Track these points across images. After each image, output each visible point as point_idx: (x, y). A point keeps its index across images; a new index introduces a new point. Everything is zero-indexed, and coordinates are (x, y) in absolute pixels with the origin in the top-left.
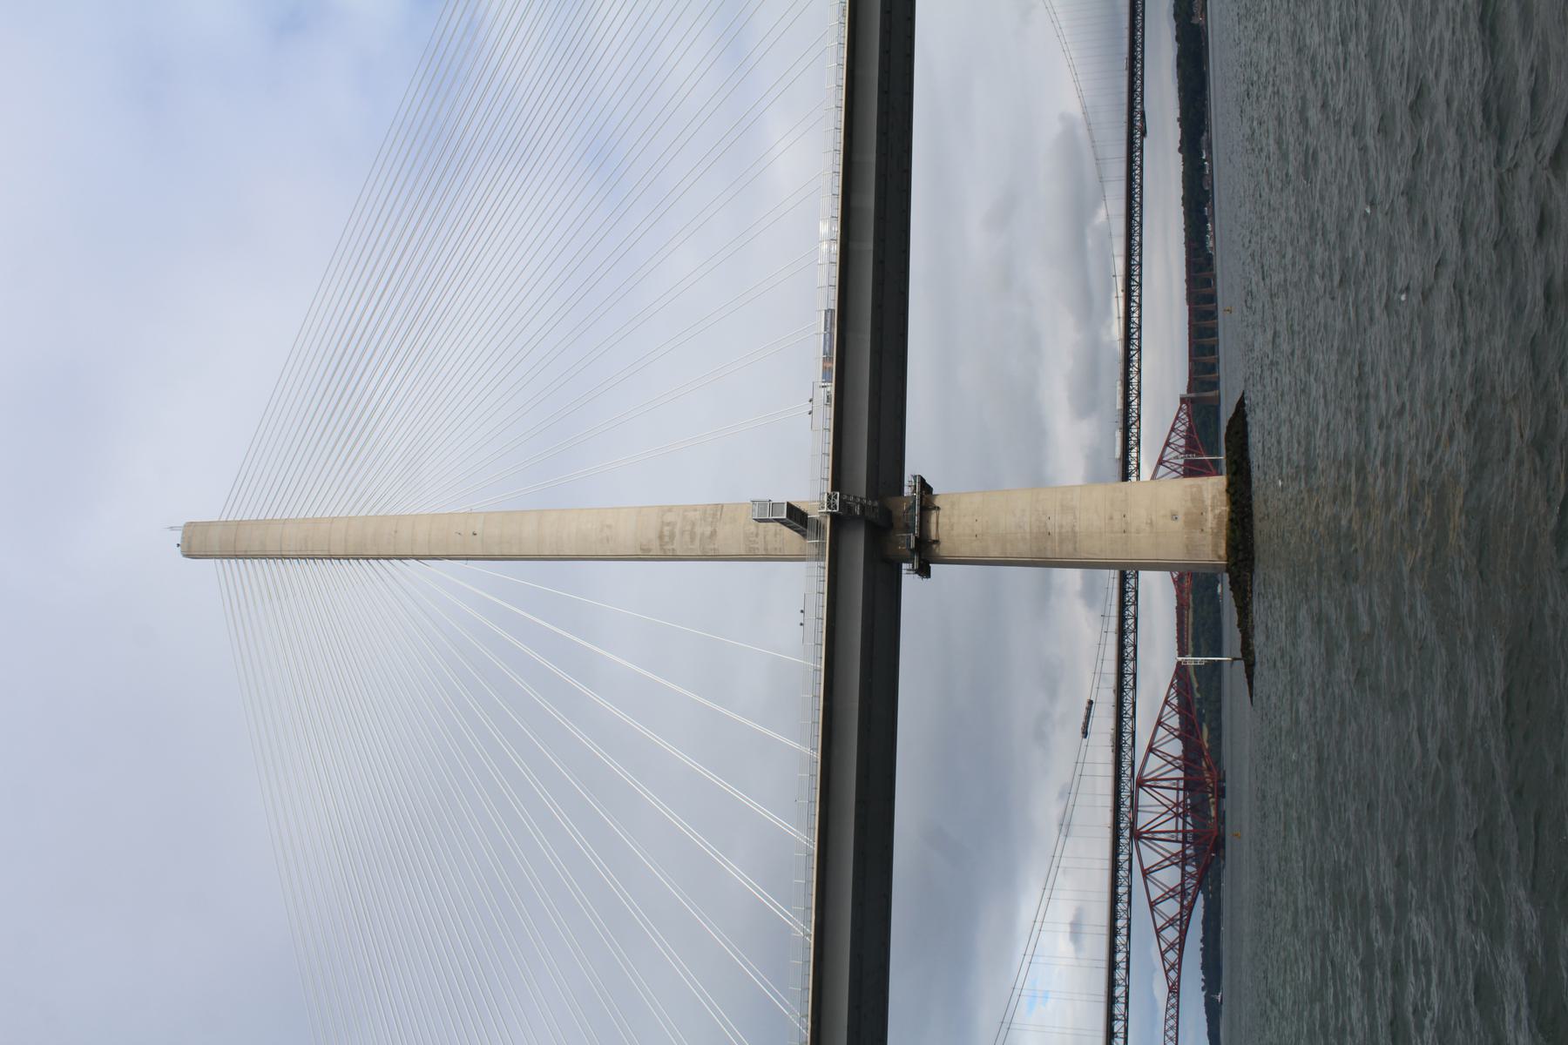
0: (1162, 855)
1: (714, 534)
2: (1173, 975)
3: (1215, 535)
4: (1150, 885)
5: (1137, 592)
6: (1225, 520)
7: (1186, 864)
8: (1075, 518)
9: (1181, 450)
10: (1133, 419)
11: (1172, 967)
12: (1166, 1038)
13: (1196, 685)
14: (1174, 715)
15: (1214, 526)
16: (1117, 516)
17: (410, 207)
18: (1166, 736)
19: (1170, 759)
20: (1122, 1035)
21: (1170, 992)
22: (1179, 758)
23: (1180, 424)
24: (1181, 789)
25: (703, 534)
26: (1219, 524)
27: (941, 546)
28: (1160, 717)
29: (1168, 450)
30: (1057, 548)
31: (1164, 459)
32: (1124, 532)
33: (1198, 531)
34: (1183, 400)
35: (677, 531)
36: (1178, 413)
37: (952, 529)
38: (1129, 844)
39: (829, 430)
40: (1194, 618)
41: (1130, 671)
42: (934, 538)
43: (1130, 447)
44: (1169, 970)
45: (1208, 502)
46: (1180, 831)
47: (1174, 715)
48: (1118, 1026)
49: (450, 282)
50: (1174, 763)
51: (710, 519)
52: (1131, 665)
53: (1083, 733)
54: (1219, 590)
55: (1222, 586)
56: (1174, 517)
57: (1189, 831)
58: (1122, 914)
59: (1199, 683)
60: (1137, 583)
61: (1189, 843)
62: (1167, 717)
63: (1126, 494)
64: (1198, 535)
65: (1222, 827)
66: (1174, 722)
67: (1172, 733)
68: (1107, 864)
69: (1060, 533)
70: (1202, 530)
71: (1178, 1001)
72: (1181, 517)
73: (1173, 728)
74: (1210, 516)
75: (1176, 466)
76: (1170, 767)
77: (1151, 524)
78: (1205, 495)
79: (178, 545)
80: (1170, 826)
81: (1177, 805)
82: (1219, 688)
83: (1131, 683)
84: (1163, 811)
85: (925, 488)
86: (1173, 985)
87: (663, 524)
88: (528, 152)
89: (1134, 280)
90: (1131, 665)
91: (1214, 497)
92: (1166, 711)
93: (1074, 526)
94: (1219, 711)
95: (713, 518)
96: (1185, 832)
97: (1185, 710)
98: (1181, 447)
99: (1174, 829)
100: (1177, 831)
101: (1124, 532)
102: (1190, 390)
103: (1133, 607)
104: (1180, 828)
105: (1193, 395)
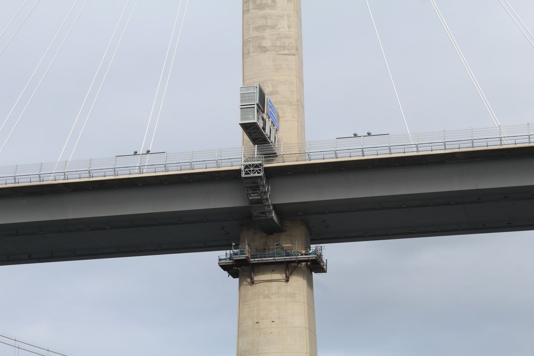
1: (264, 49)
25: (263, 38)
35: (267, 11)
42: (256, 278)
95: (280, 46)
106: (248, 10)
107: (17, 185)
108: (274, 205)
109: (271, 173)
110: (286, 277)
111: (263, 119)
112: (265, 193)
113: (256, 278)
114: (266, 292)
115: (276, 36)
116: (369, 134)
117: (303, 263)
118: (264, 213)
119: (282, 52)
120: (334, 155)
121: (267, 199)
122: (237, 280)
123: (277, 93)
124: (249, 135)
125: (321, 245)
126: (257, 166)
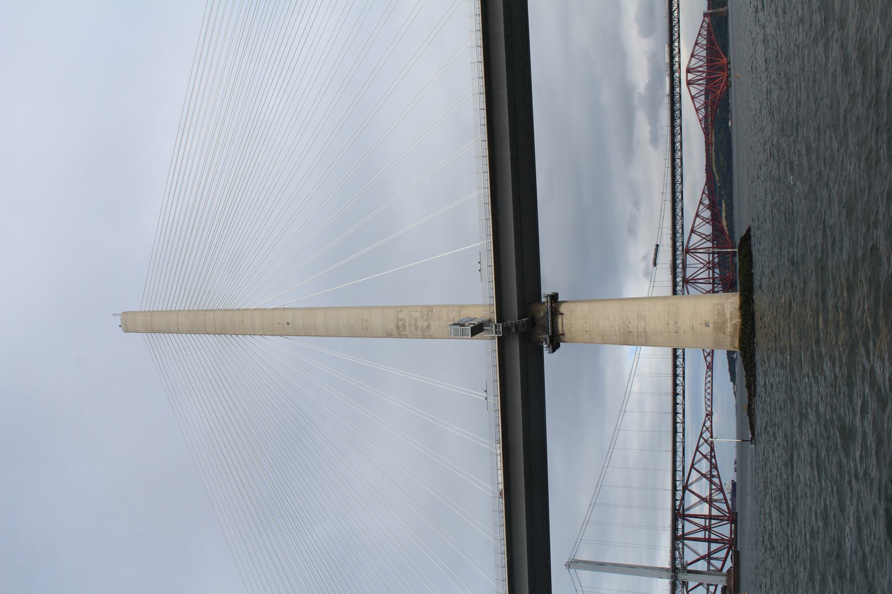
0: (700, 103)
1: (429, 326)
2: (709, 359)
3: (732, 336)
4: (695, 102)
5: (680, 96)
6: (738, 327)
7: (715, 268)
8: (646, 323)
9: (705, 29)
10: (675, 7)
11: (709, 354)
12: (706, 393)
13: (717, 179)
14: (705, 210)
15: (732, 331)
16: (672, 322)
17: (191, 262)
18: (702, 223)
19: (704, 236)
20: (682, 357)
21: (708, 368)
22: (709, 236)
23: (704, 30)
24: (711, 253)
25: (422, 326)
26: (735, 330)
27: (566, 336)
28: (697, 212)
29: (697, 47)
30: (636, 340)
31: (695, 54)
32: (676, 332)
33: (722, 333)
34: (705, 15)
35: (407, 324)
36: (702, 24)
37: (572, 327)
38: (681, 236)
39: (482, 78)
40: (715, 139)
41: (679, 157)
42: (561, 332)
43: (674, 24)
44: (707, 356)
45: (728, 316)
46: (711, 278)
47: (705, 210)
48: (679, 371)
49: (228, 198)
50: (706, 238)
51: (426, 318)
52: (679, 153)
53: (654, 264)
54: (730, 125)
55: (731, 122)
56: (707, 325)
57: (716, 278)
58: (679, 292)
59: (719, 177)
60: (681, 122)
61: (716, 284)
62: (698, 100)
63: (677, 308)
64: (721, 336)
65: (735, 274)
66: (707, 202)
67: (705, 207)
68: (670, 284)
69: (637, 332)
70: (724, 333)
71: (712, 373)
72: (711, 325)
73: (705, 218)
74: (729, 325)
75: (702, 58)
76: (704, 240)
77: (693, 328)
78: (726, 311)
79: (120, 326)
80: (705, 275)
81: (709, 263)
82: (731, 181)
83: (680, 164)
84: (702, 267)
85: (554, 297)
86: (709, 364)
87: (398, 320)
88: (254, 126)
89: (675, 80)
90: (679, 153)
91: (731, 313)
92: (696, 49)
93: (645, 328)
94: (731, 194)
95: (427, 317)
96: (714, 278)
97: (712, 207)
98: (705, 45)
99: (707, 277)
100: (709, 278)
101: (676, 332)
102: (709, 8)
103: (679, 120)
104: (711, 276)
105: (711, 11)
106: (406, 335)
107: (505, 525)
108: (519, 319)
109: (500, 318)
110: (560, 314)
111: (469, 324)
112: (511, 323)
113: (561, 332)
114: (569, 326)
115: (421, 319)
116: (479, 263)
117: (553, 305)
118: (523, 325)
119: (431, 316)
120: (492, 298)
121: (515, 322)
122: (561, 344)
123: (454, 319)
124: (477, 333)
125: (542, 294)
126: (496, 327)
